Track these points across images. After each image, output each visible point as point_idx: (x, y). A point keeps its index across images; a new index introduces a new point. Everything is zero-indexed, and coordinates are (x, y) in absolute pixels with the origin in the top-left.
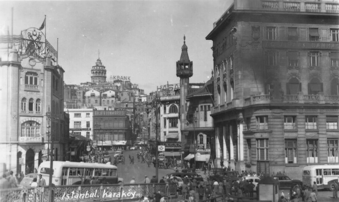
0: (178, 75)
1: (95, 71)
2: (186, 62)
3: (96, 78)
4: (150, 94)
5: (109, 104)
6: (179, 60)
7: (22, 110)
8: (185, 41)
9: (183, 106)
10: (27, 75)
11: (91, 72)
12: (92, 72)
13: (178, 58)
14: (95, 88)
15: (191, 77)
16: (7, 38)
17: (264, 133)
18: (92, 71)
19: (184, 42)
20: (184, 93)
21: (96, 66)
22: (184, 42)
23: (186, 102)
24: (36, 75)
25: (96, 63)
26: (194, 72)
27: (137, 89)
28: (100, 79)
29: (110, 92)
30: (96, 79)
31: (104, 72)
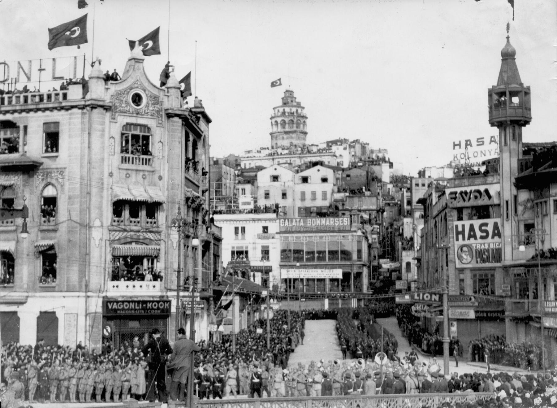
0: (492, 124)
1: (279, 120)
2: (514, 86)
3: (281, 136)
4: (420, 173)
5: (306, 201)
6: (495, 84)
7: (68, 278)
8: (510, 35)
9: (507, 202)
10: (532, 153)
11: (270, 121)
12: (273, 120)
13: (492, 81)
14: (282, 161)
15: (527, 126)
16: (194, 213)
17: (196, 151)
18: (271, 118)
19: (508, 38)
20: (508, 169)
21: (281, 107)
22: (508, 38)
23: (514, 191)
24: (252, 268)
25: (295, 98)
26: (535, 112)
27: (386, 162)
28: (292, 138)
29: (319, 170)
30: (283, 138)
31: (302, 120)
